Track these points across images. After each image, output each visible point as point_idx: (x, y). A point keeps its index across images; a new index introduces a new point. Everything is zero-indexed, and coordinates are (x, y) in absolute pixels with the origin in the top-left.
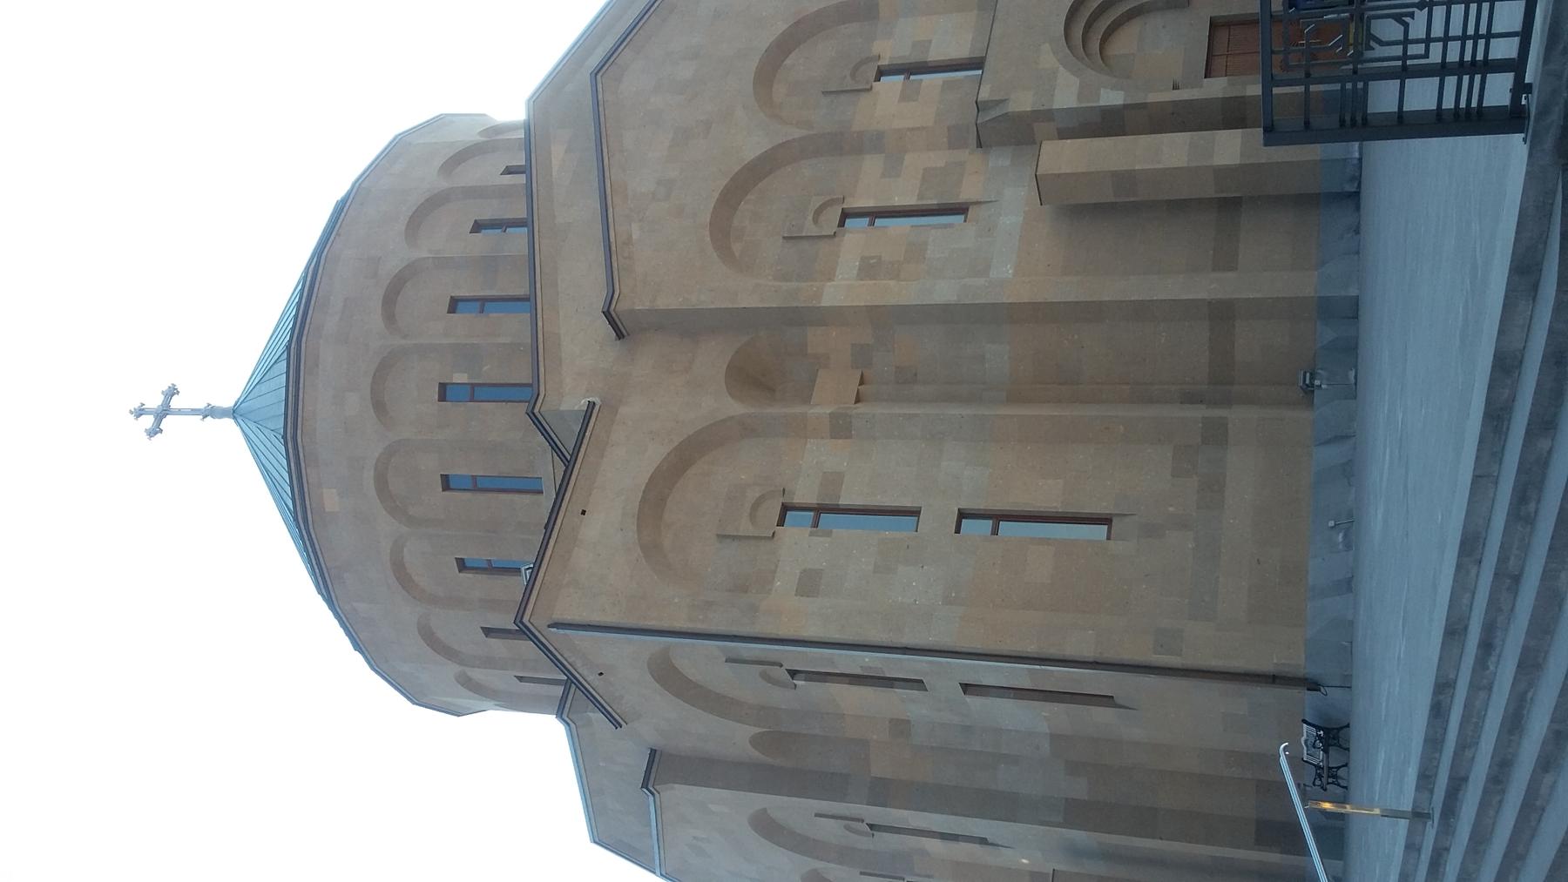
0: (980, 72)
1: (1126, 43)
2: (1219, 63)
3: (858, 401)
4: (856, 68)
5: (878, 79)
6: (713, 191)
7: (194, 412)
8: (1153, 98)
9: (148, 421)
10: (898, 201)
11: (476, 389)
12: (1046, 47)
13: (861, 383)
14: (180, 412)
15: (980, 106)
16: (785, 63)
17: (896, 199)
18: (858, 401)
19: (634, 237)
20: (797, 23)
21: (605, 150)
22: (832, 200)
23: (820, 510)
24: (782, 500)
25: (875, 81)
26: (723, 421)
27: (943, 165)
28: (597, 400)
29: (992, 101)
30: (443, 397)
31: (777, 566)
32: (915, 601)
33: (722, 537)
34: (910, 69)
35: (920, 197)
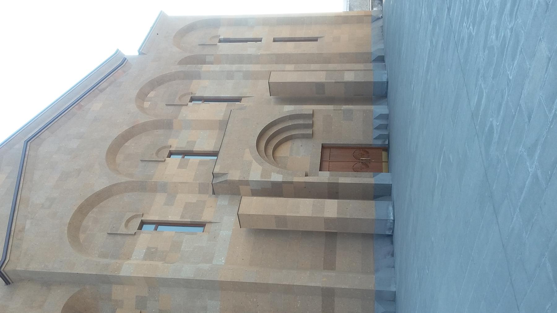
0: (216, 158)
1: (284, 151)
2: (326, 164)
4: (159, 150)
5: (169, 156)
8: (296, 179)
10: (171, 218)
15: (214, 175)
17: (170, 217)
19: (27, 227)
20: (133, 127)
21: (22, 180)
29: (220, 173)
35: (182, 217)
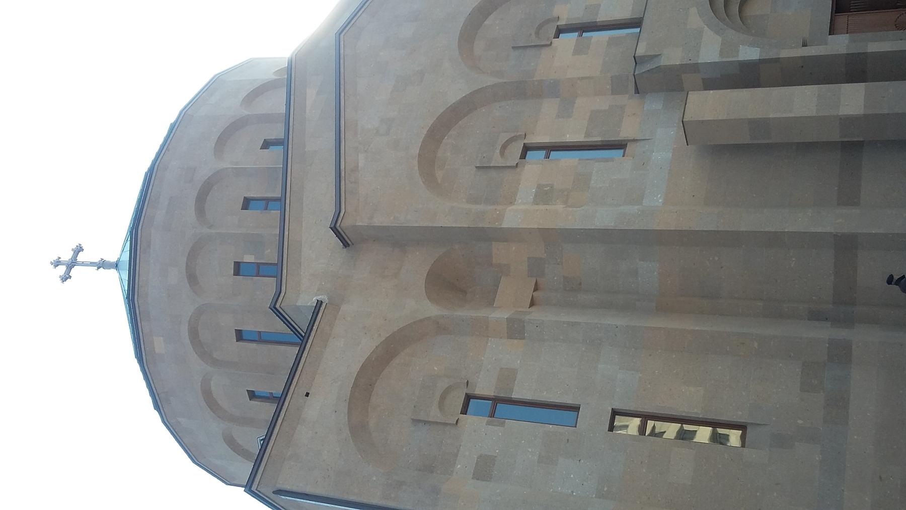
0: (638, 30)
3: (532, 304)
4: (540, 27)
5: (557, 36)
6: (423, 128)
7: (92, 264)
8: (785, 54)
9: (62, 269)
10: (570, 138)
11: (261, 267)
12: (694, 10)
13: (536, 289)
14: (83, 264)
15: (637, 60)
16: (485, 22)
17: (568, 136)
18: (532, 304)
21: (342, 94)
22: (516, 136)
23: (496, 401)
24: (465, 391)
25: (554, 38)
26: (421, 321)
27: (607, 108)
28: (323, 297)
30: (237, 272)
31: (458, 451)
32: (573, 492)
33: (416, 421)
34: (583, 28)
